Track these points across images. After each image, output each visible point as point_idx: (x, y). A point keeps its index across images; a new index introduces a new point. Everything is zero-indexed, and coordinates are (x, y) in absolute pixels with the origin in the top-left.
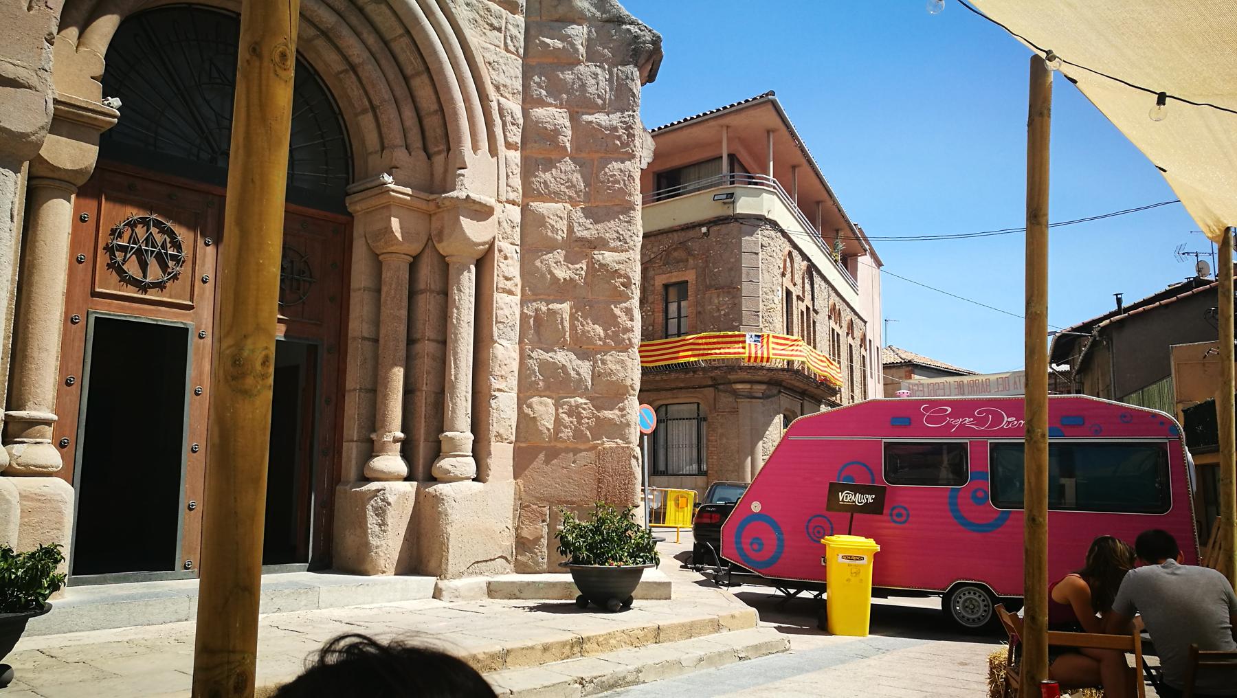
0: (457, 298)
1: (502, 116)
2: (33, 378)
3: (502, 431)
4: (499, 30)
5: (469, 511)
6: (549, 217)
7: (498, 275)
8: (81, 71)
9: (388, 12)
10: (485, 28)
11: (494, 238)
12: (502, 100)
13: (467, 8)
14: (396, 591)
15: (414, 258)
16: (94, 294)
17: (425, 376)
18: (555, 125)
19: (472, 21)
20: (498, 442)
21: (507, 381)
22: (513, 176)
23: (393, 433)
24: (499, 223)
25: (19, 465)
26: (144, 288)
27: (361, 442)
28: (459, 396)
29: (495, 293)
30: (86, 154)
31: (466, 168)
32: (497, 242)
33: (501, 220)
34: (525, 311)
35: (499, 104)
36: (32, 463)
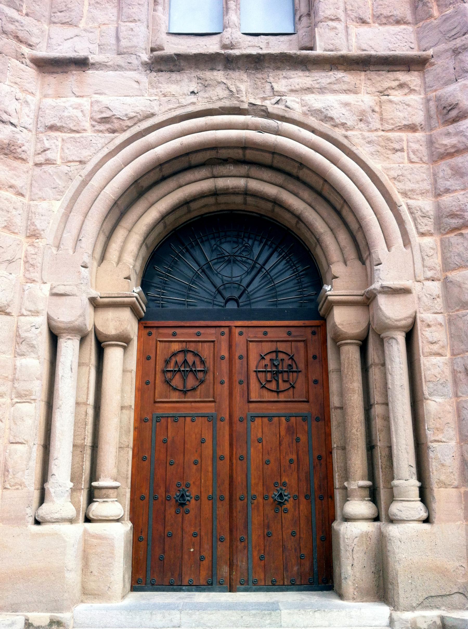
0: (390, 367)
1: (411, 213)
2: (102, 461)
3: (443, 478)
4: (402, 150)
5: (416, 550)
6: (464, 283)
7: (423, 342)
8: (118, 276)
9: (308, 172)
10: (388, 154)
11: (416, 312)
12: (410, 202)
13: (369, 145)
14: (352, 618)
15: (362, 341)
16: (155, 402)
17: (378, 433)
18: (460, 205)
19: (374, 153)
20: (441, 487)
21: (443, 433)
22: (428, 258)
23: (357, 482)
24: (419, 298)
25: (93, 515)
26: (185, 392)
27: (342, 489)
28: (400, 449)
29: (422, 357)
30: (123, 323)
31: (380, 264)
32: (418, 315)
33: (420, 296)
34: (455, 368)
35: (408, 205)
36: (99, 514)
